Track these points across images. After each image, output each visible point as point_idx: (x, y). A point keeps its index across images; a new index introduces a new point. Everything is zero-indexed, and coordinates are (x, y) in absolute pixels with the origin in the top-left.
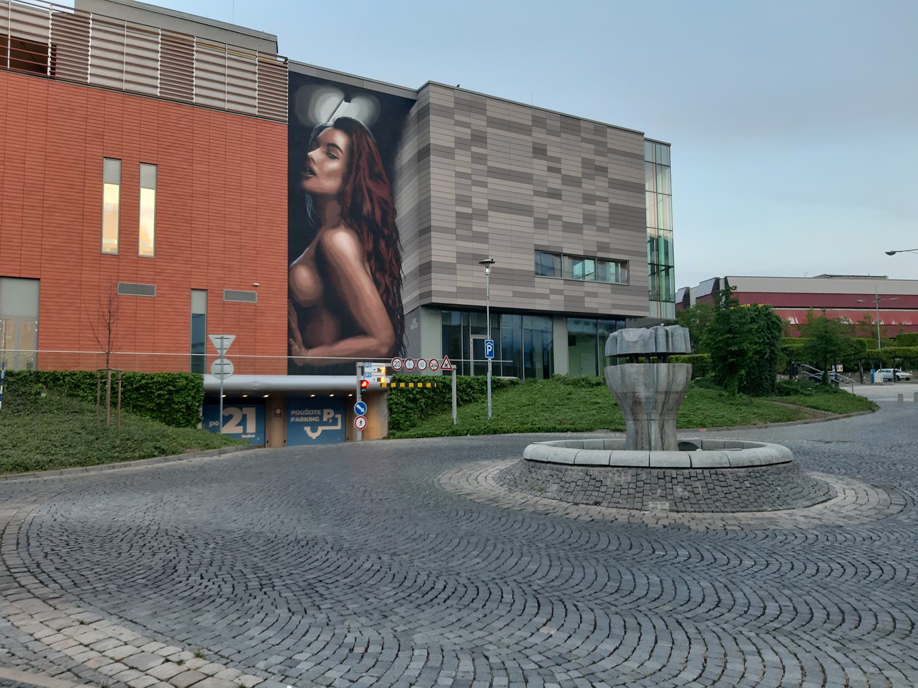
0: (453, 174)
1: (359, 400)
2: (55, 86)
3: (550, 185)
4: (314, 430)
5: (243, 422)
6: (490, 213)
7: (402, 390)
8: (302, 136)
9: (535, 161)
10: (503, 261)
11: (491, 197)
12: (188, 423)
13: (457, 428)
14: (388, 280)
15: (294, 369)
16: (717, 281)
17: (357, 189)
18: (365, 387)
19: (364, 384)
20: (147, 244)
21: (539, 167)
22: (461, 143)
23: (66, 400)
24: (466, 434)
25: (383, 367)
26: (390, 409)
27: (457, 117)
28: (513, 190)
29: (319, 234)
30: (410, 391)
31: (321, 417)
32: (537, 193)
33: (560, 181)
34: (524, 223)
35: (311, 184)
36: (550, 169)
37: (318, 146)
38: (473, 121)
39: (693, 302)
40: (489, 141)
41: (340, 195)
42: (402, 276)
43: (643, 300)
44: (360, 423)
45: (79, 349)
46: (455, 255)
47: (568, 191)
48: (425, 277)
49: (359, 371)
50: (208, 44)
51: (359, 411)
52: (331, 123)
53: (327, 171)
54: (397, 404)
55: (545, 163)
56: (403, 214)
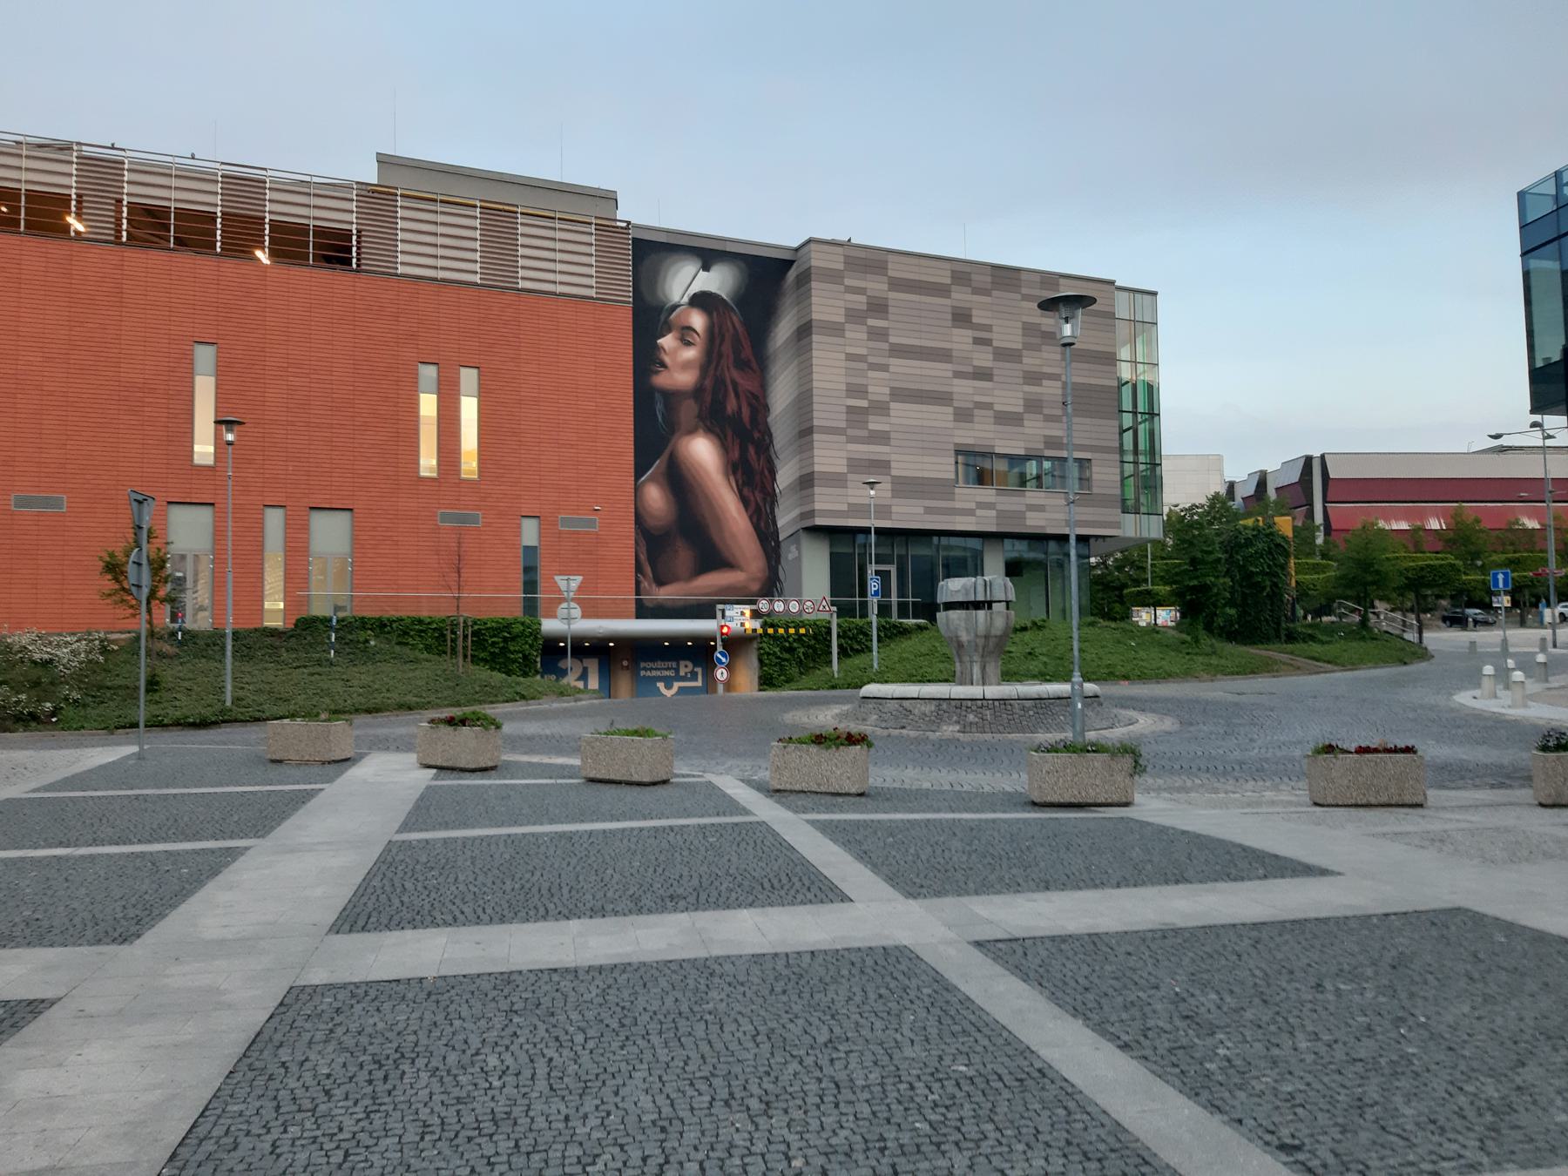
0: (843, 356)
1: (720, 648)
3: (976, 363)
4: (669, 687)
6: (893, 405)
7: (774, 637)
8: (650, 318)
9: (956, 331)
10: (905, 466)
12: (525, 675)
14: (759, 497)
16: (1308, 460)
17: (719, 383)
19: (725, 630)
20: (469, 463)
21: (961, 340)
22: (853, 316)
23: (398, 649)
25: (747, 610)
26: (761, 661)
27: (847, 282)
31: (677, 670)
32: (958, 375)
33: (991, 357)
34: (940, 416)
35: (662, 380)
37: (669, 331)
38: (870, 285)
39: (1272, 494)
40: (891, 310)
41: (697, 392)
43: (1115, 513)
44: (721, 674)
45: (397, 590)
46: (845, 462)
47: (1003, 369)
48: (805, 492)
49: (719, 614)
52: (686, 299)
53: (681, 362)
55: (969, 333)
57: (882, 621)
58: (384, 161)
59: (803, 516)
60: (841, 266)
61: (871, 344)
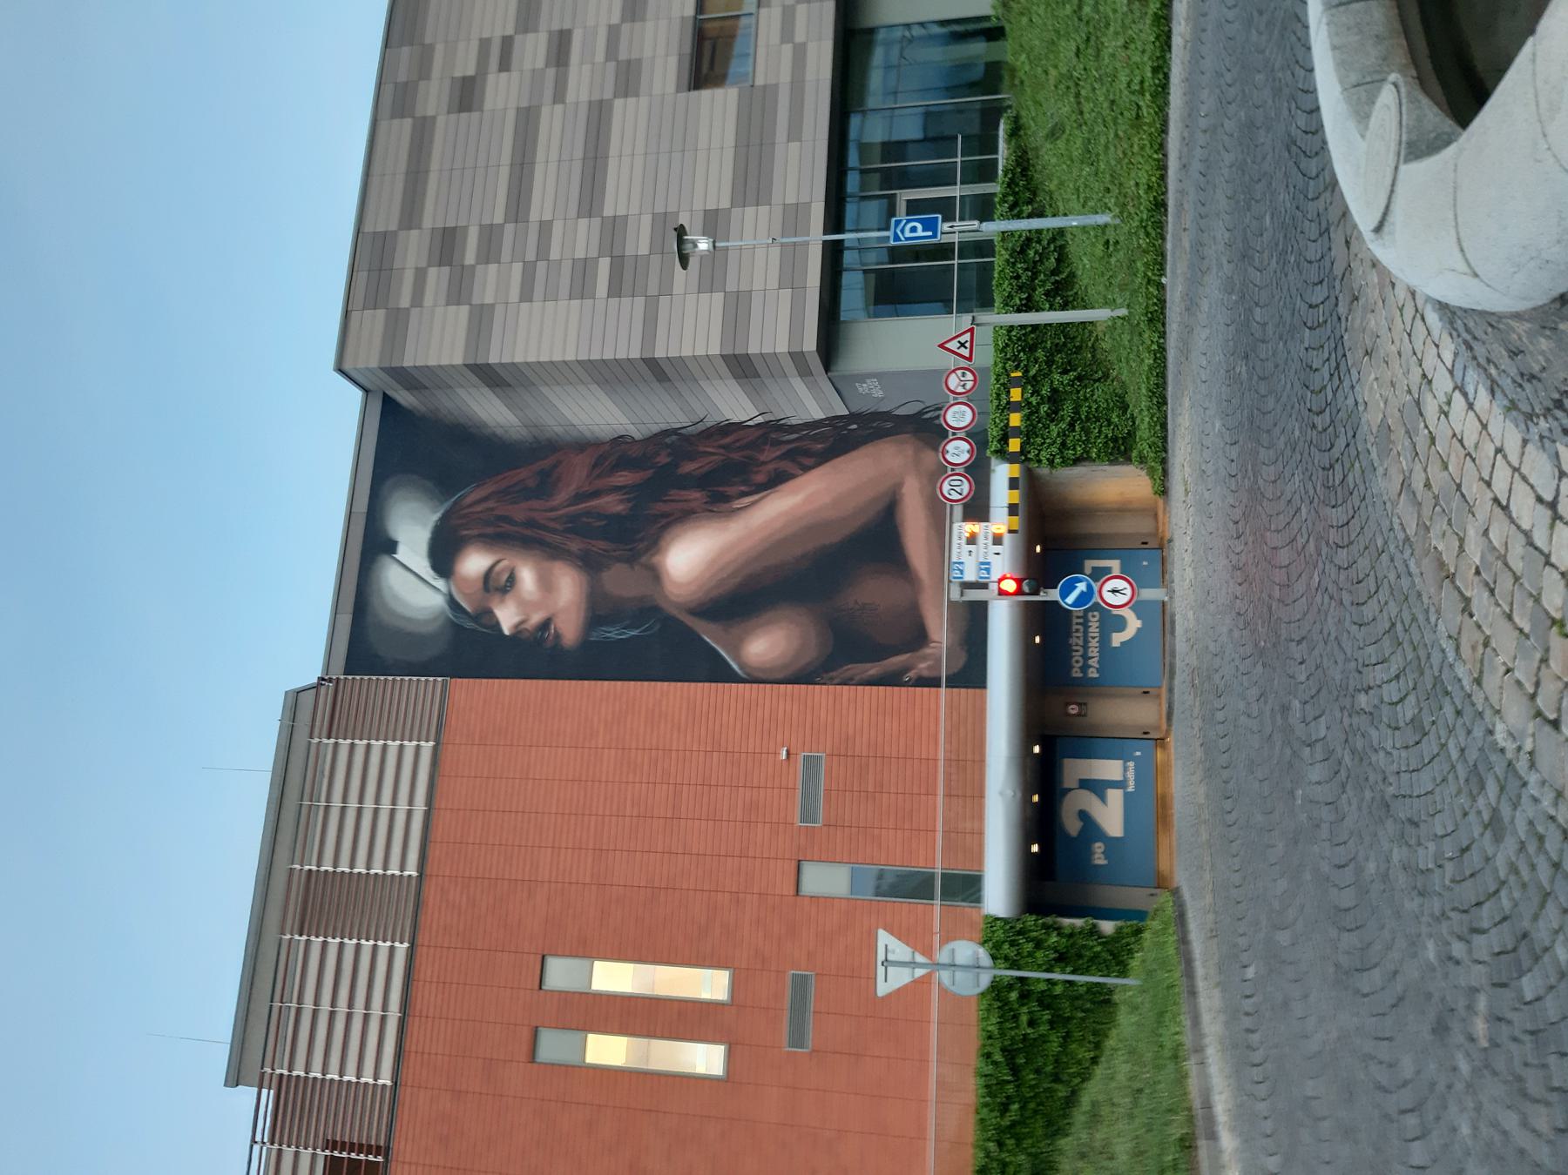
0: (525, 305)
2: (401, 1147)
3: (540, 63)
5: (1098, 788)
6: (608, 211)
7: (1028, 434)
8: (472, 646)
9: (488, 105)
10: (712, 185)
11: (573, 212)
13: (1139, 310)
14: (768, 454)
15: (972, 674)
17: (576, 526)
18: (1019, 582)
19: (1010, 586)
21: (502, 93)
22: (458, 292)
24: (1161, 287)
26: (1077, 461)
27: (405, 302)
28: (554, 156)
29: (674, 612)
30: (1031, 413)
32: (559, 97)
33: (531, 36)
34: (628, 117)
35: (569, 629)
36: (505, 66)
41: (589, 564)
42: (760, 419)
46: (705, 297)
49: (975, 595)
50: (300, 844)
51: (1084, 598)
52: (440, 584)
53: (540, 593)
54: (1063, 444)
55: (491, 78)
56: (624, 420)
57: (1001, 209)
58: (235, 1078)
59: (804, 372)
60: (381, 313)
61: (506, 254)
